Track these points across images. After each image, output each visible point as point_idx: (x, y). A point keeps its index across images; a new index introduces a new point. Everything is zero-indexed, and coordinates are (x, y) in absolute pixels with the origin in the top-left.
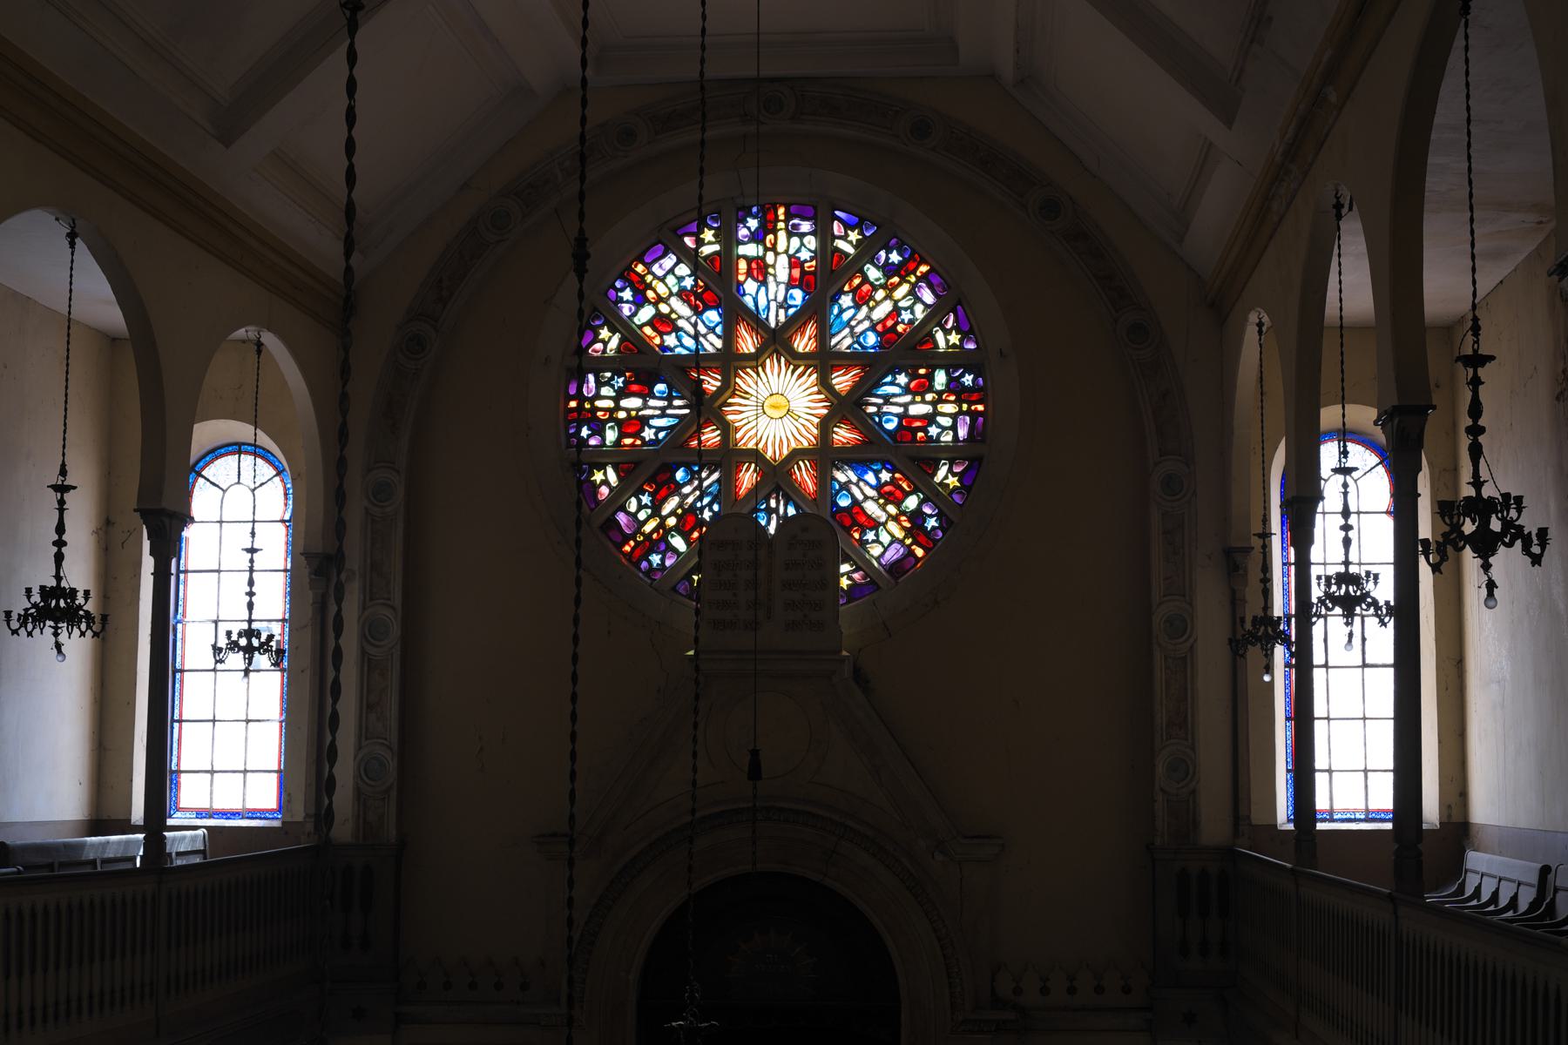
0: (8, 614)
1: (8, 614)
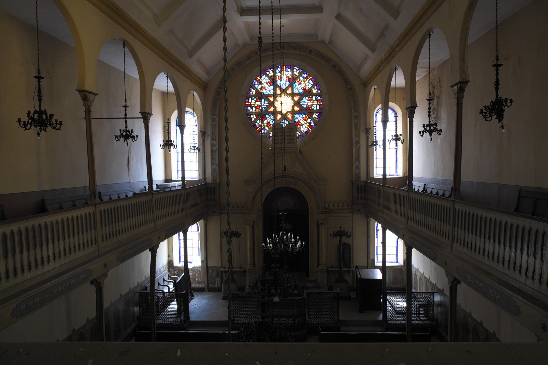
0: (161, 145)
1: (161, 145)
